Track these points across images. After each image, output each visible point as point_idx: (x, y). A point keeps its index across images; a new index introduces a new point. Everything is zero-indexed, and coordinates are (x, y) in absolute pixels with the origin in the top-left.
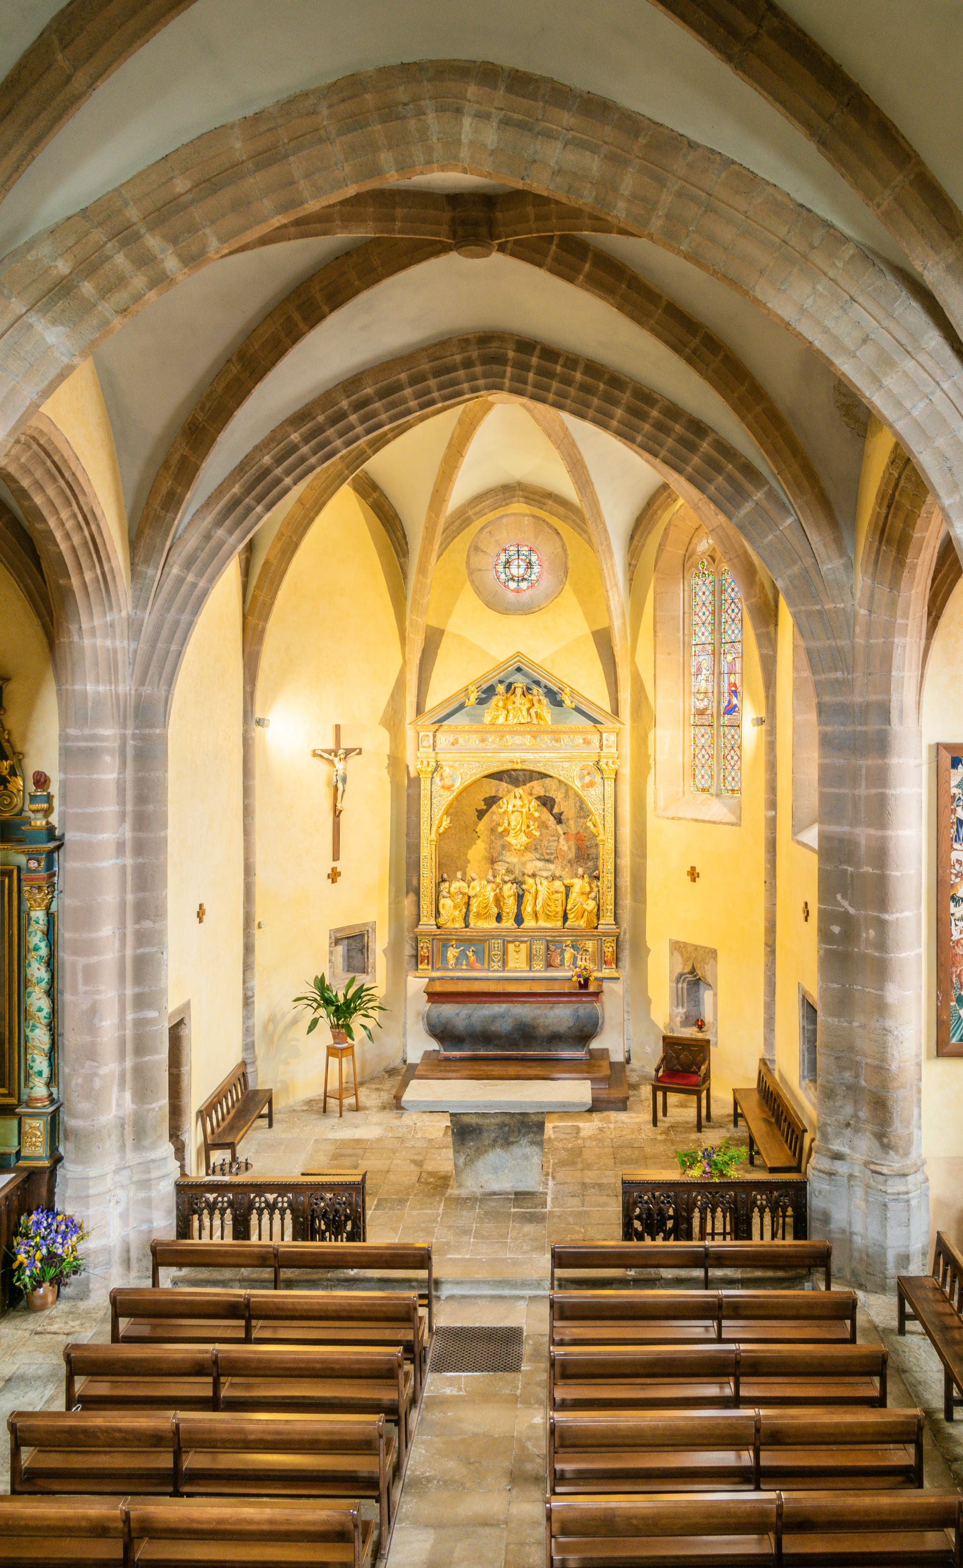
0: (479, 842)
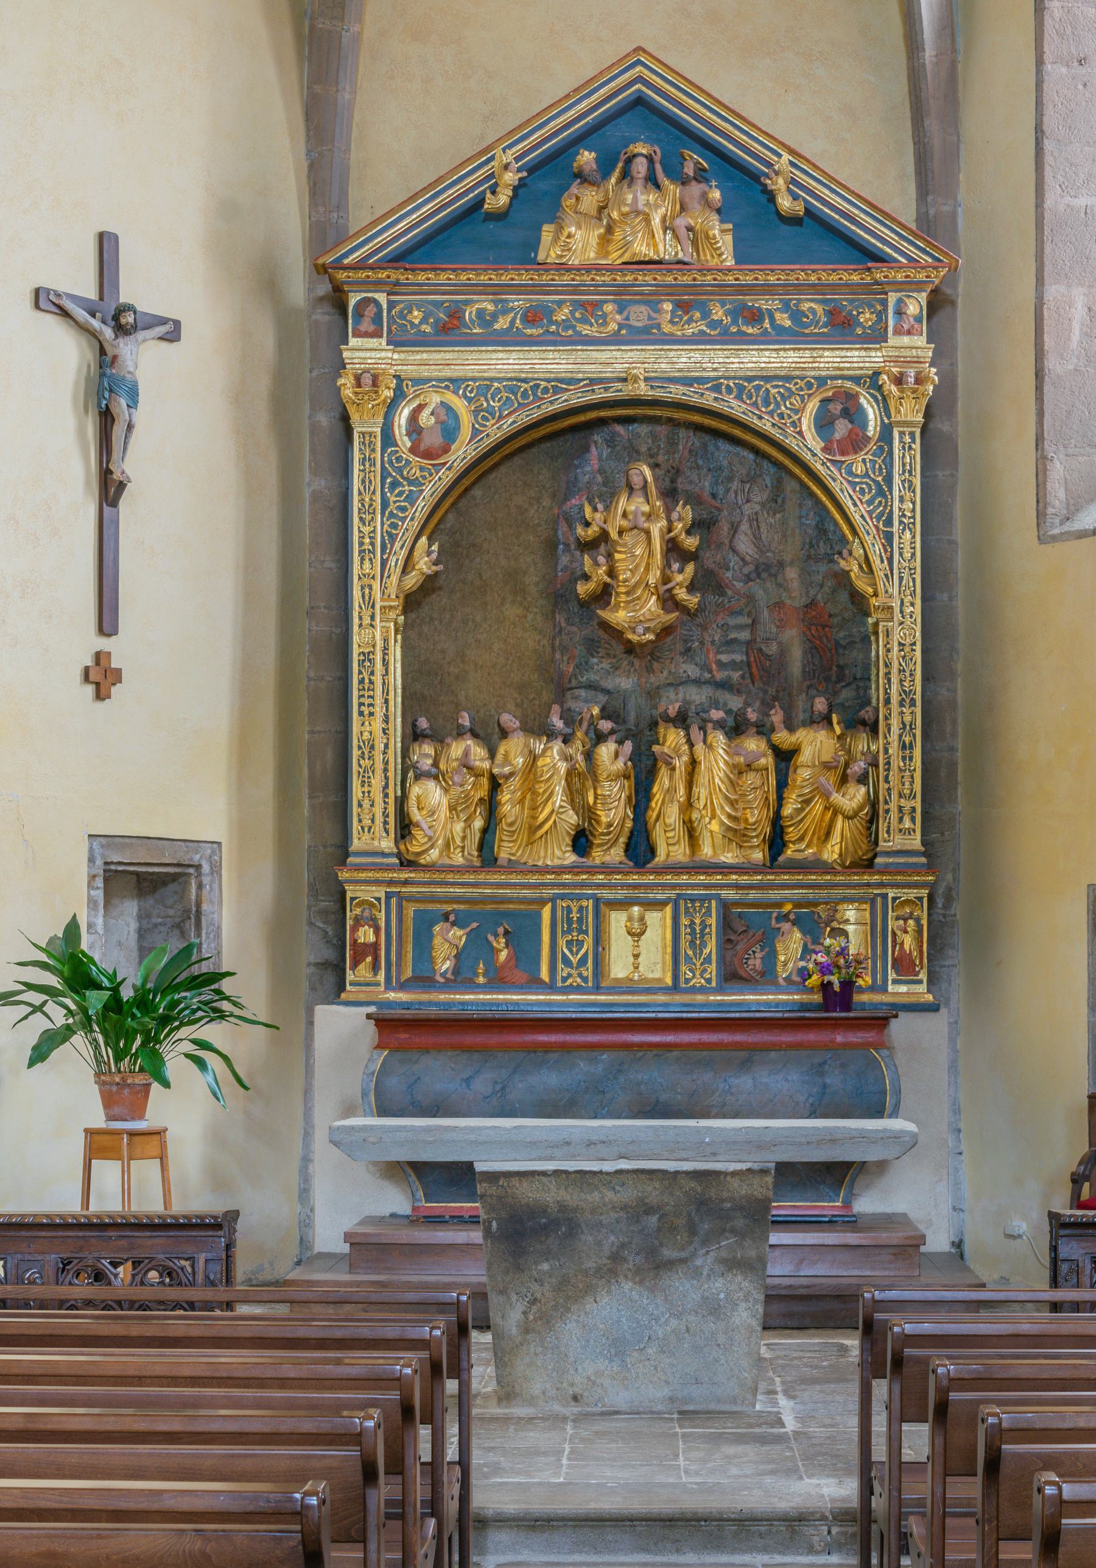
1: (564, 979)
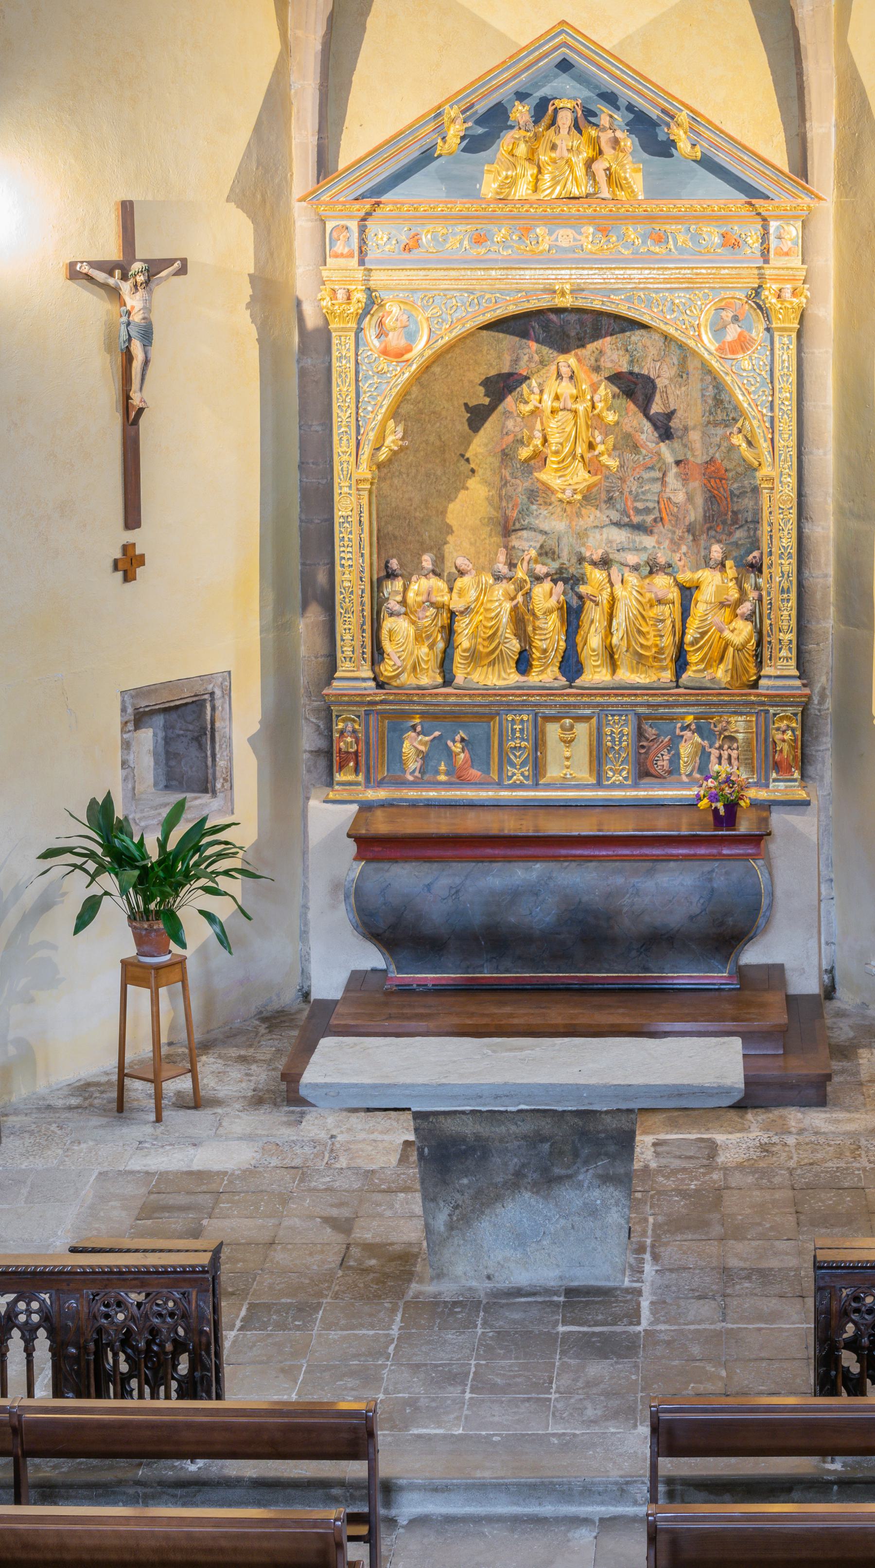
0: (472, 483)
1: (510, 778)
